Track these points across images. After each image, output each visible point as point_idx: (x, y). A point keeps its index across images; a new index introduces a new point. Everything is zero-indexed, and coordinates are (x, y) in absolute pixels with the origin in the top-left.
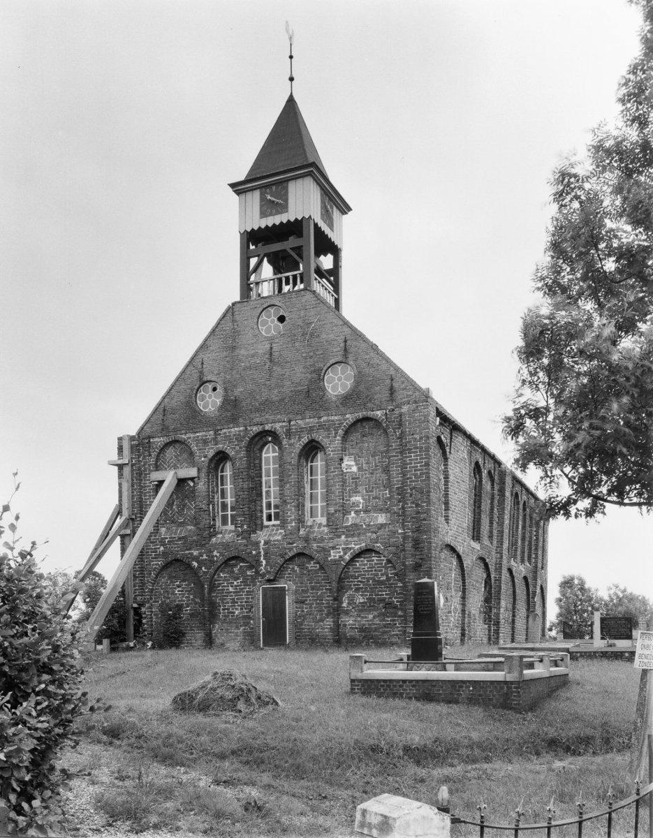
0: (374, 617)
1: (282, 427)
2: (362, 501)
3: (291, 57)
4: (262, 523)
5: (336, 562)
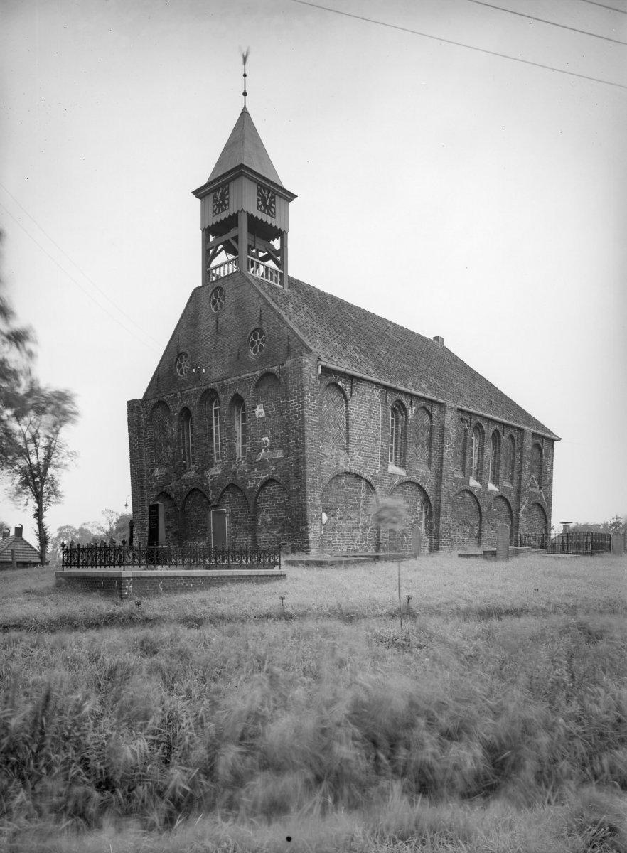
0: (277, 533)
2: (268, 440)
4: (213, 461)
5: (252, 490)
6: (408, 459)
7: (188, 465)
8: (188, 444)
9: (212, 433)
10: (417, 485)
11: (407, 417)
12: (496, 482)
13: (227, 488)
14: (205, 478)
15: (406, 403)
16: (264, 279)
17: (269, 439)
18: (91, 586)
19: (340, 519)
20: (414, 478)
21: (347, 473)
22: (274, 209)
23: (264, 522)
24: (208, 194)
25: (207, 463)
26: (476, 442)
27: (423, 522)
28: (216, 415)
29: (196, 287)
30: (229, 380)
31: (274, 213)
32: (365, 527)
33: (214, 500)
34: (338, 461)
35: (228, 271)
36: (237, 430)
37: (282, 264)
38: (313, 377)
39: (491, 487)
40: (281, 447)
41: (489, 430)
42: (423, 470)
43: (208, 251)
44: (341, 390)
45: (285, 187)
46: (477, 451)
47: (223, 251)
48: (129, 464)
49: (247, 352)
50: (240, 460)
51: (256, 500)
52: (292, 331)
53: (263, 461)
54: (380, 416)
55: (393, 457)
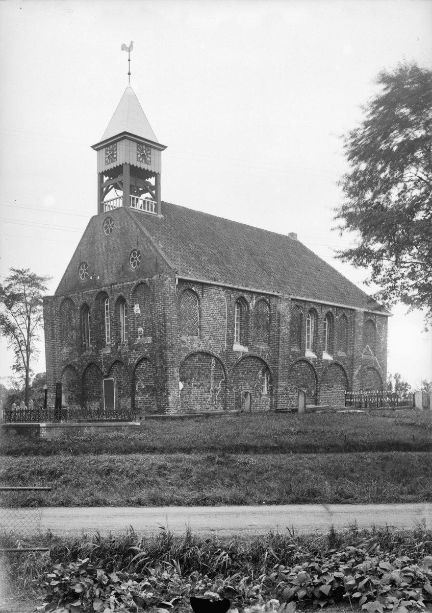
1: (108, 289)
2: (142, 330)
3: (129, 60)
6: (250, 339)
7: (87, 345)
8: (88, 329)
9: (104, 322)
10: (258, 358)
11: (248, 308)
12: (331, 352)
13: (114, 363)
14: (99, 355)
15: (248, 299)
16: (143, 210)
17: (143, 329)
18: (360, 376)
19: (195, 385)
20: (256, 354)
21: (199, 352)
22: (150, 158)
23: (140, 389)
24: (102, 148)
25: (100, 343)
26: (312, 322)
27: (265, 385)
28: (107, 310)
29: (92, 216)
30: (115, 286)
31: (150, 161)
32: (215, 391)
33: (105, 371)
34: (192, 344)
35: (119, 205)
36: (122, 321)
37: (156, 197)
38: (172, 287)
39: (326, 356)
40: (151, 335)
41: (322, 313)
42: (263, 347)
43: (102, 189)
44: (195, 293)
45: (159, 143)
46: (313, 330)
47: (114, 188)
48: (44, 343)
49: (129, 266)
50: (124, 343)
51: (134, 372)
52: (158, 253)
53: (139, 345)
54: (226, 310)
55: (239, 338)
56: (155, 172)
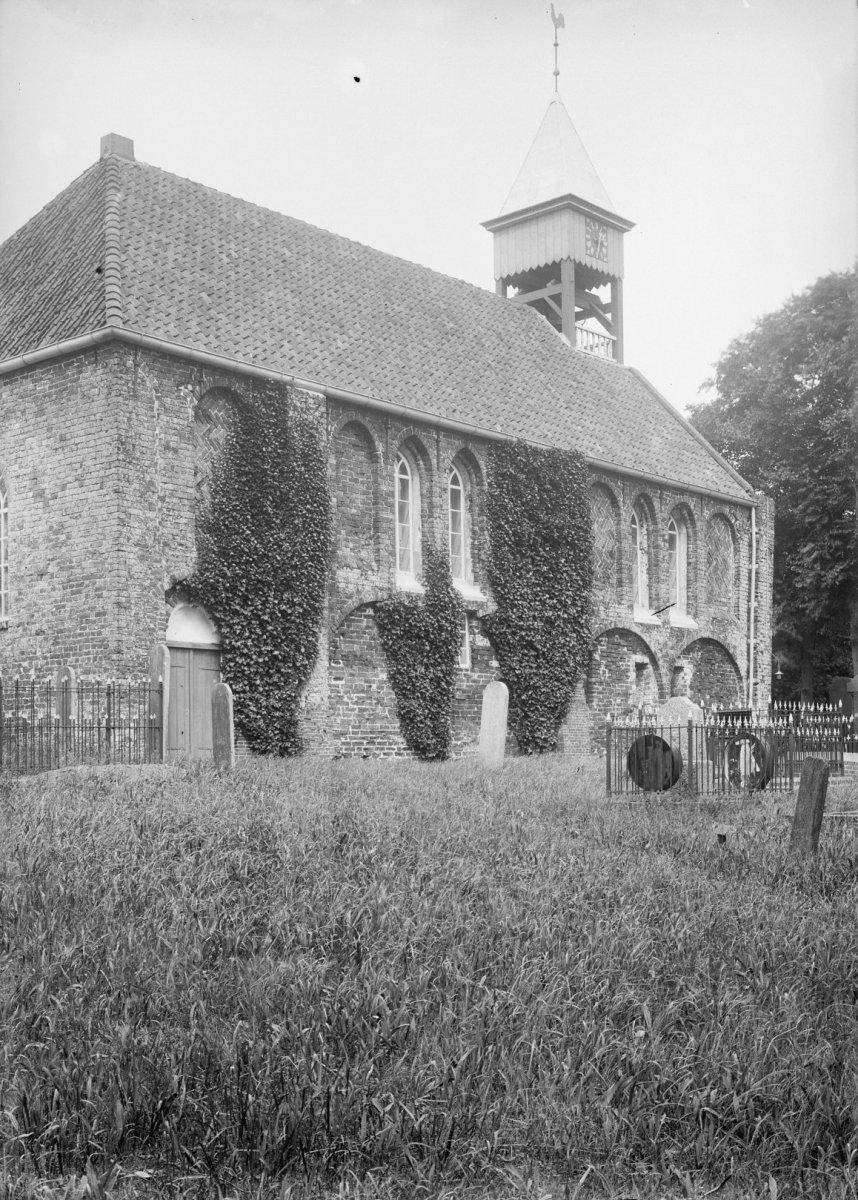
56: (614, 276)
